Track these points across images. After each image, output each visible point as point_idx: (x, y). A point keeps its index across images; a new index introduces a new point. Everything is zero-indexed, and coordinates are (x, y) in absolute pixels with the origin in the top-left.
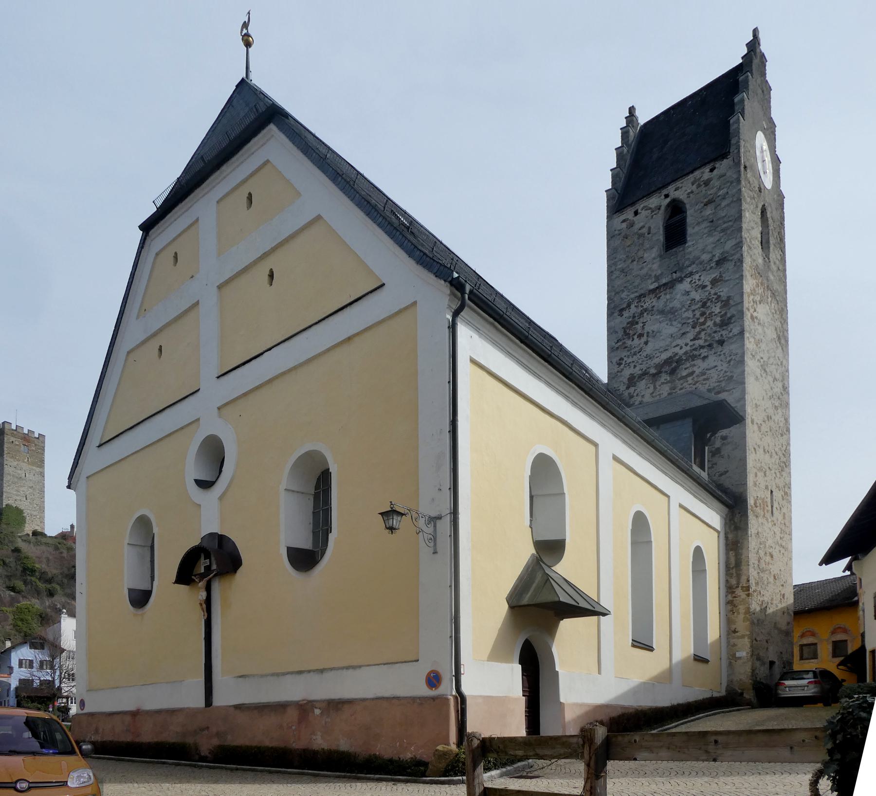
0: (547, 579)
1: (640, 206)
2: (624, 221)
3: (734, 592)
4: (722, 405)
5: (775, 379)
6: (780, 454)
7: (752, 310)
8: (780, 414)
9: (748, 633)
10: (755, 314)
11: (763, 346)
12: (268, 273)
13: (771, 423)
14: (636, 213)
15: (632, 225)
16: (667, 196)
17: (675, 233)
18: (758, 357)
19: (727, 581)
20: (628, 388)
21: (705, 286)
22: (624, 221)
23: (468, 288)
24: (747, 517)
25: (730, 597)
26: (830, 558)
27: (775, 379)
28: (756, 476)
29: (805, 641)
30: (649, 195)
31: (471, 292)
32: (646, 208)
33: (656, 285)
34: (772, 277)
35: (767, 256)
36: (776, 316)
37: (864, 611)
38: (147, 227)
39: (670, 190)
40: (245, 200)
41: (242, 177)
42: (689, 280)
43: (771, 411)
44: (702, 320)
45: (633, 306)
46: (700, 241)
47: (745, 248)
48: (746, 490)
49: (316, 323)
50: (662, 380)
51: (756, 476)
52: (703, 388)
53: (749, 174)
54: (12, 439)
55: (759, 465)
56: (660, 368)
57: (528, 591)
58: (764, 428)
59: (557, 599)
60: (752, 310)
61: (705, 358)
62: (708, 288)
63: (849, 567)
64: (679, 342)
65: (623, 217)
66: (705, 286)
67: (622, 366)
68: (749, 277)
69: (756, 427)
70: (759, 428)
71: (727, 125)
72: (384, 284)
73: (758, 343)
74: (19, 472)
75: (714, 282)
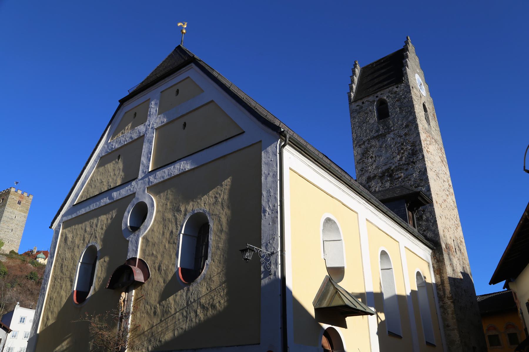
0: (337, 291)
1: (365, 100)
2: (357, 106)
3: (443, 300)
4: (418, 194)
5: (444, 181)
6: (454, 220)
7: (426, 148)
8: (450, 198)
9: (456, 327)
10: (428, 150)
11: (435, 164)
12: (183, 123)
13: (446, 203)
14: (363, 103)
15: (362, 107)
16: (377, 97)
17: (383, 112)
18: (434, 170)
19: (438, 293)
20: (367, 183)
21: (402, 136)
22: (357, 106)
23: (288, 136)
24: (443, 254)
25: (441, 304)
26: (494, 281)
27: (444, 181)
28: (444, 231)
29: (491, 333)
30: (368, 96)
31: (290, 138)
32: (368, 101)
33: (377, 134)
34: (433, 133)
35: (429, 124)
36: (439, 151)
37: (522, 313)
38: (123, 101)
39: (379, 94)
40: (175, 92)
41: (176, 82)
42: (393, 133)
43: (445, 197)
44: (402, 151)
45: (366, 143)
46: (394, 111)
47: (418, 120)
48: (439, 239)
49: (207, 148)
50: (386, 179)
51: (444, 231)
52: (408, 184)
53: (415, 90)
54: (14, 197)
55: (444, 226)
56: (383, 173)
57: (326, 298)
58: (444, 206)
59: (340, 303)
60: (426, 148)
61: (407, 169)
62: (404, 137)
63: (506, 286)
64: (392, 161)
65: (357, 104)
66: (402, 136)
67: (363, 172)
68: (422, 133)
69: (439, 206)
70: (441, 206)
71: (402, 71)
72: (244, 132)
73: (432, 163)
74: (12, 215)
75: (406, 134)
